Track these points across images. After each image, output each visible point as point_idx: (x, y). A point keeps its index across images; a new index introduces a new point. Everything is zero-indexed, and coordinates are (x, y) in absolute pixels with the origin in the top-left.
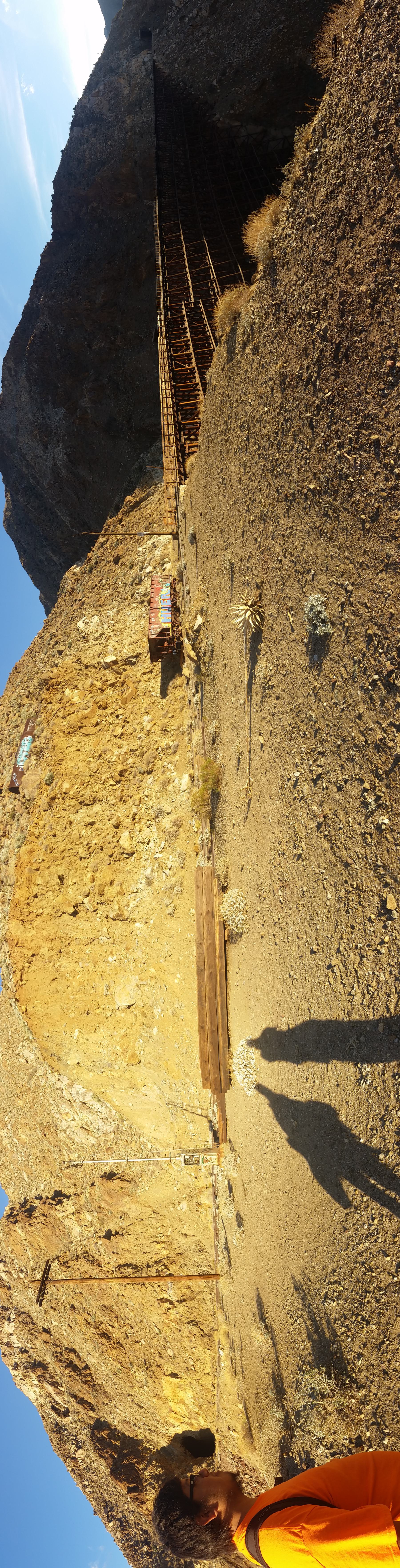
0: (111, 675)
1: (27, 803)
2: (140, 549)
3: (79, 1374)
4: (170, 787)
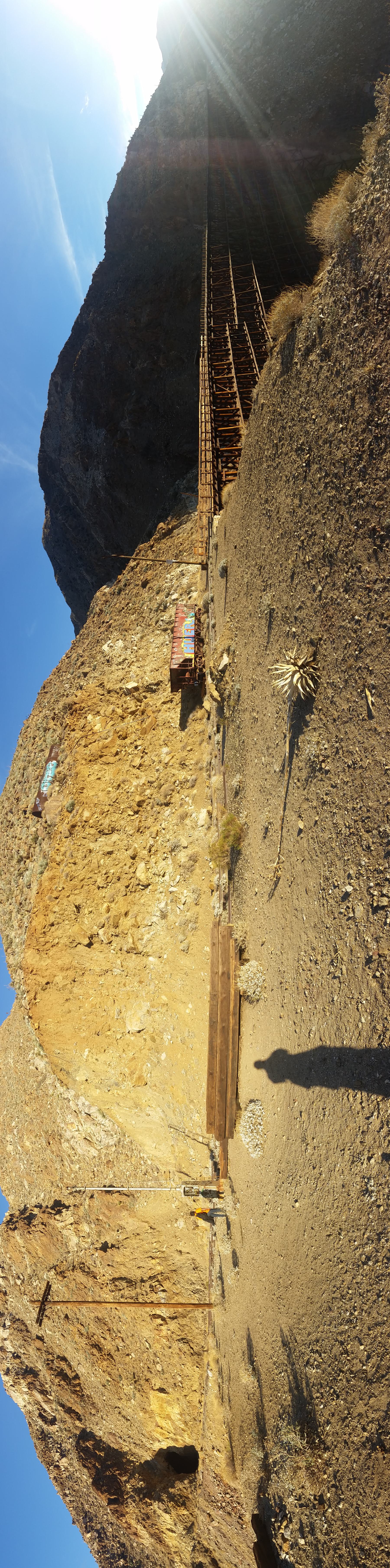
0: (132, 702)
1: (49, 827)
2: (169, 576)
3: (69, 1384)
4: (187, 821)
